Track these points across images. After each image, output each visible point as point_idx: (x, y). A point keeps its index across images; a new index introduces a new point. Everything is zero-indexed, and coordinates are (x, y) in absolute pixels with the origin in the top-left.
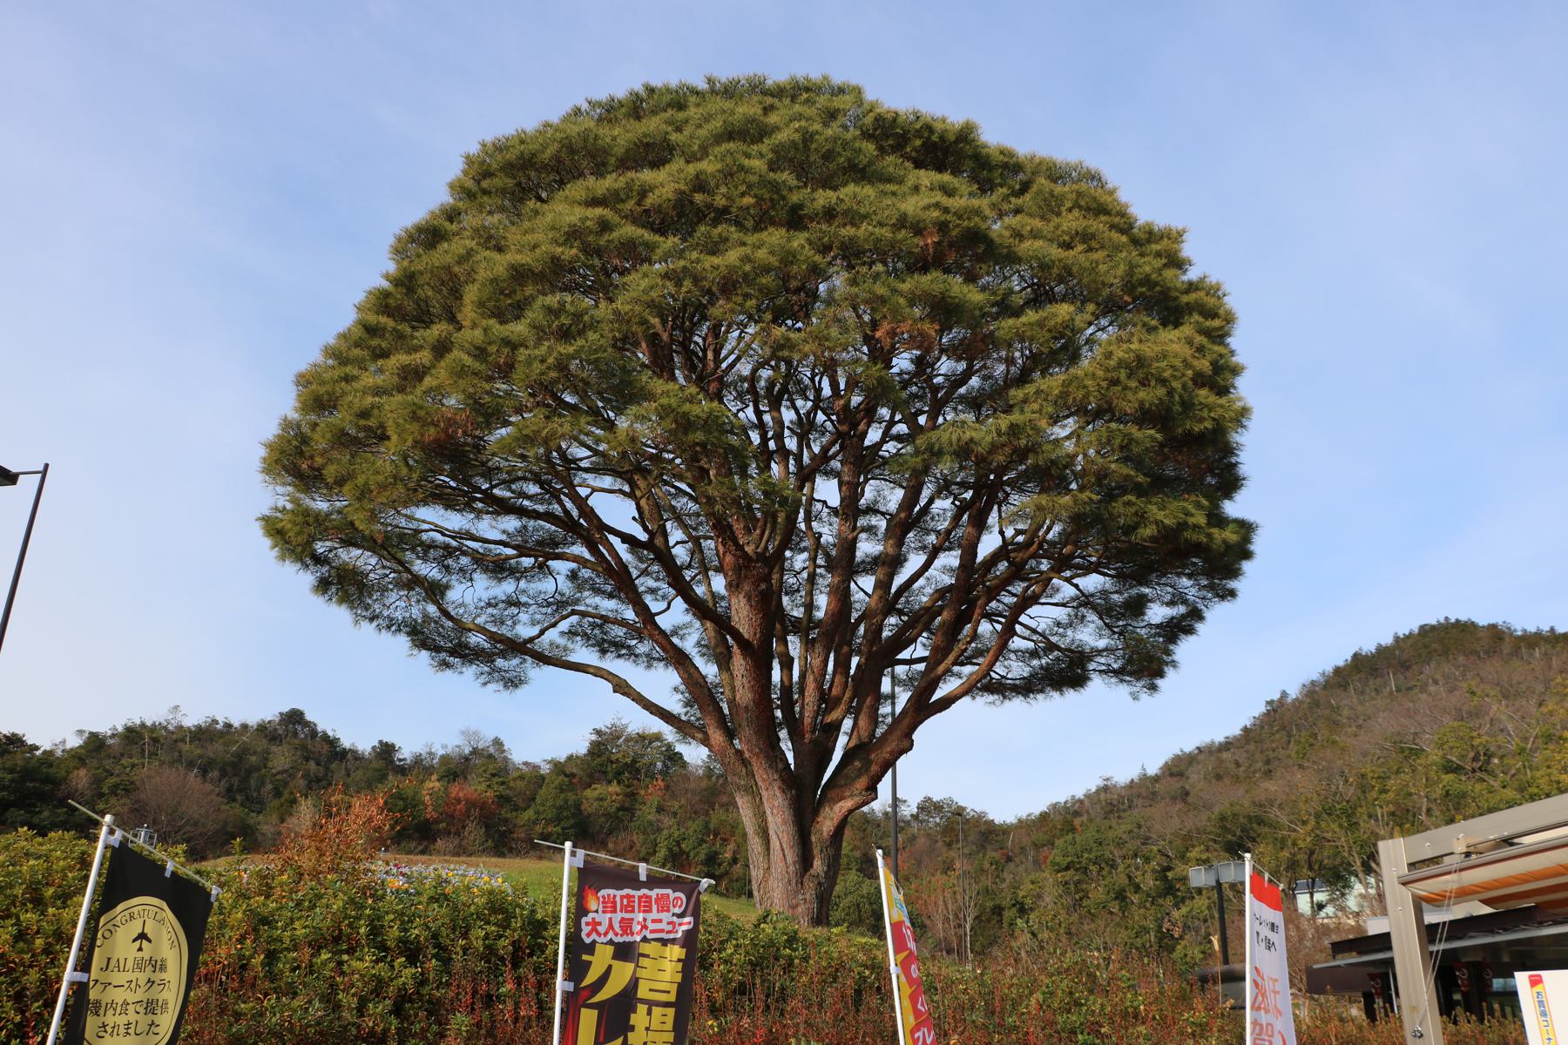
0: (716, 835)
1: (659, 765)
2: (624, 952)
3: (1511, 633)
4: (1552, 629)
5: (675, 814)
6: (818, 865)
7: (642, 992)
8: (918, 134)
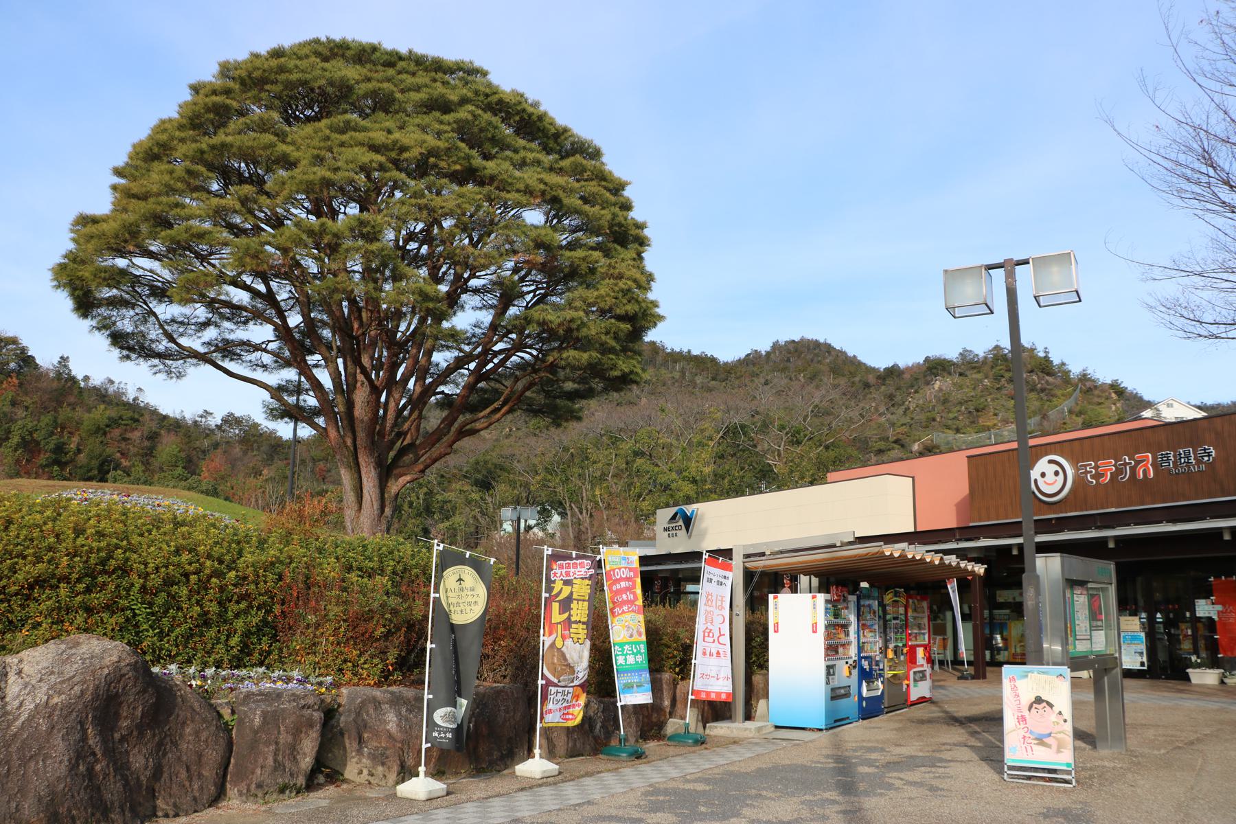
0: (63, 428)
1: (12, 365)
2: (568, 583)
3: (664, 349)
4: (689, 352)
5: (27, 408)
6: (388, 511)
7: (575, 596)
8: (518, 113)
